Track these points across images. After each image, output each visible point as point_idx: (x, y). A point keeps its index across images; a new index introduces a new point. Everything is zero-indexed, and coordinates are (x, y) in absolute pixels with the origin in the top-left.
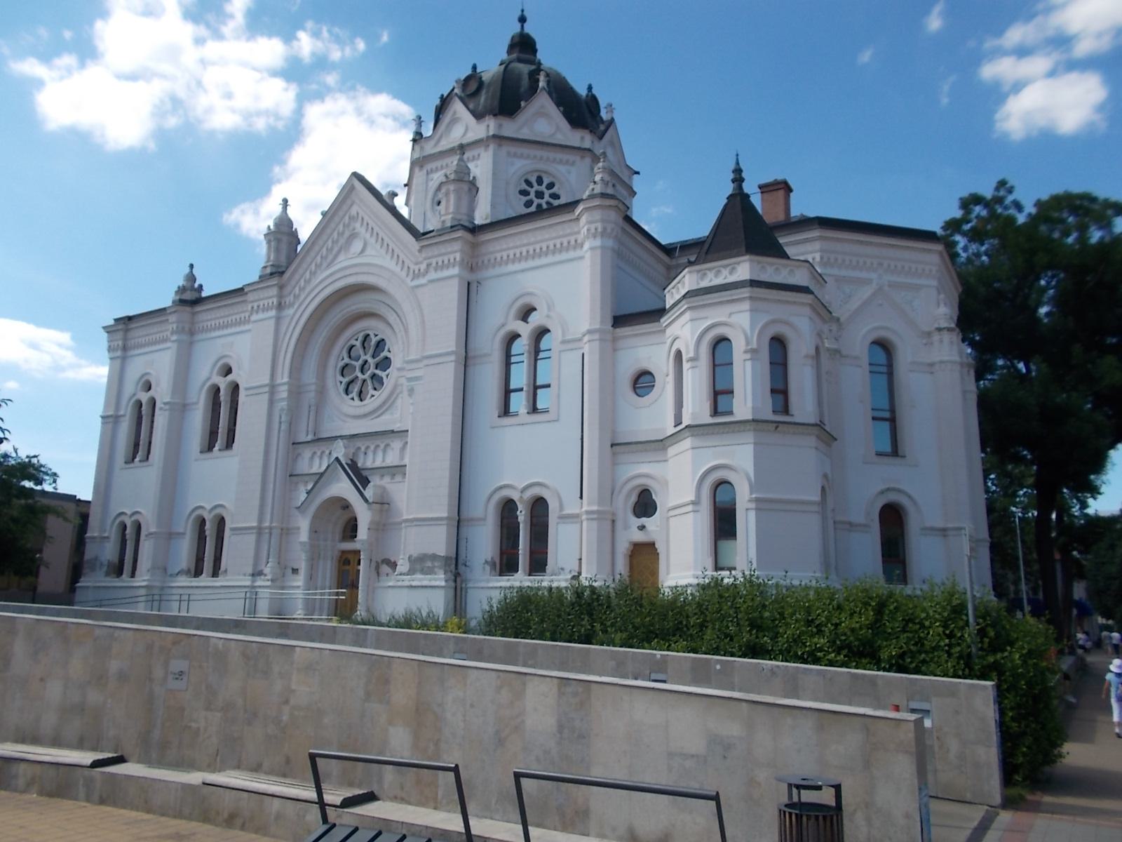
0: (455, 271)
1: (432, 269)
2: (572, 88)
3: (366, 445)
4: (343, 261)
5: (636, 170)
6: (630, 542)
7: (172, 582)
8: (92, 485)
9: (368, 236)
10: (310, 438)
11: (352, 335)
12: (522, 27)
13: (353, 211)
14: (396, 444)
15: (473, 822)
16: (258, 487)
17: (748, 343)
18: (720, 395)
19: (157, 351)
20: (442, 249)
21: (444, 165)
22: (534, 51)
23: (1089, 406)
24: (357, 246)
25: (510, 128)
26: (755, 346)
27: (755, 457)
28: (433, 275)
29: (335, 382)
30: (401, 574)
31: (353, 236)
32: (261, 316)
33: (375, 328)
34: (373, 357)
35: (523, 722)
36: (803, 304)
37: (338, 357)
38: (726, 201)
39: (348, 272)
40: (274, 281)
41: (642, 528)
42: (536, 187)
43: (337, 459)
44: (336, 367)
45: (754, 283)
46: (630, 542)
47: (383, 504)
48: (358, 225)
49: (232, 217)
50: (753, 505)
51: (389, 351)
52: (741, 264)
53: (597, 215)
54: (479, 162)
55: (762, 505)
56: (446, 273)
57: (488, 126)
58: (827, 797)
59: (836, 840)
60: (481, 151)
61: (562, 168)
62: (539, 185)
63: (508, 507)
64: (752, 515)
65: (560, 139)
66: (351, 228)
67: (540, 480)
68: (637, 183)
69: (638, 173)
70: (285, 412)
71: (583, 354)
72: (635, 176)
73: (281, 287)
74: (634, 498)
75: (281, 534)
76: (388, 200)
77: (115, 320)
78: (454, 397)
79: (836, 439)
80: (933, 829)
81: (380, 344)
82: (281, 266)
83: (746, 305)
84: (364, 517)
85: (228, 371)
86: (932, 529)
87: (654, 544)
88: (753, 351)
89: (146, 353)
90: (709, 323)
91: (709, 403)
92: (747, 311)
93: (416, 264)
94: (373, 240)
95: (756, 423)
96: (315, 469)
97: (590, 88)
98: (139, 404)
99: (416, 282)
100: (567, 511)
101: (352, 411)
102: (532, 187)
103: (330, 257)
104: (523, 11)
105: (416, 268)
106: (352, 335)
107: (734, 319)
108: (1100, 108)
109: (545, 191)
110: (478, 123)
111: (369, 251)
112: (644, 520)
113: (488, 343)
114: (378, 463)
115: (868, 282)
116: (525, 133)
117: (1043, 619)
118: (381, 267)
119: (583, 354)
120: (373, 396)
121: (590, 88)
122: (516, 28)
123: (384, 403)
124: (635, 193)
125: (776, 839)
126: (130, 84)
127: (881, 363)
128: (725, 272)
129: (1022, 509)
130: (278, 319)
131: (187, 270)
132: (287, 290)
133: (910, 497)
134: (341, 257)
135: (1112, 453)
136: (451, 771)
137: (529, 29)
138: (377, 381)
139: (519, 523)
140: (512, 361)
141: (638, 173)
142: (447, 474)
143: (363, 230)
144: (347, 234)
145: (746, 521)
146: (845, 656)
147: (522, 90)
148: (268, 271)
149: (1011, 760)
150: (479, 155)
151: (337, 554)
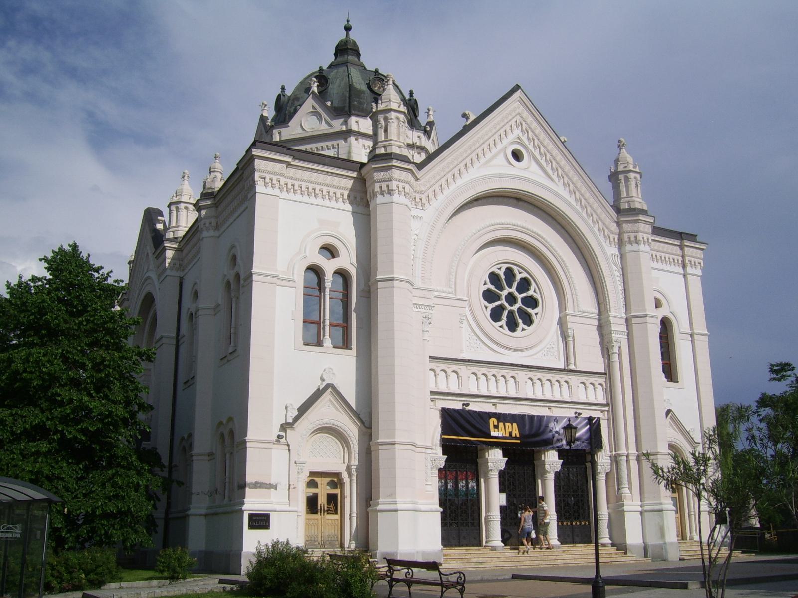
2: (307, 505)
7: (295, 146)
8: (661, 368)
12: (347, 35)
15: (408, 589)
16: (671, 246)
19: (443, 399)
21: (760, 442)
23: (43, 332)
34: (511, 313)
38: (462, 128)
42: (513, 290)
49: (758, 525)
51: (501, 327)
59: (720, 596)
62: (517, 289)
69: (259, 541)
78: (378, 478)
79: (696, 236)
80: (551, 541)
82: (122, 281)
89: (476, 401)
92: (698, 276)
97: (411, 93)
98: (315, 270)
102: (510, 286)
104: (348, 21)
108: (298, 548)
110: (338, 256)
117: (118, 314)
121: (411, 93)
122: (342, 35)
125: (592, 597)
126: (291, 451)
127: (339, 290)
129: (560, 524)
131: (279, 92)
135: (297, 413)
136: (346, 36)
137: (353, 35)
139: (507, 317)
140: (507, 424)
142: (380, 415)
146: (777, 455)
148: (246, 174)
149: (106, 282)
151: (566, 547)
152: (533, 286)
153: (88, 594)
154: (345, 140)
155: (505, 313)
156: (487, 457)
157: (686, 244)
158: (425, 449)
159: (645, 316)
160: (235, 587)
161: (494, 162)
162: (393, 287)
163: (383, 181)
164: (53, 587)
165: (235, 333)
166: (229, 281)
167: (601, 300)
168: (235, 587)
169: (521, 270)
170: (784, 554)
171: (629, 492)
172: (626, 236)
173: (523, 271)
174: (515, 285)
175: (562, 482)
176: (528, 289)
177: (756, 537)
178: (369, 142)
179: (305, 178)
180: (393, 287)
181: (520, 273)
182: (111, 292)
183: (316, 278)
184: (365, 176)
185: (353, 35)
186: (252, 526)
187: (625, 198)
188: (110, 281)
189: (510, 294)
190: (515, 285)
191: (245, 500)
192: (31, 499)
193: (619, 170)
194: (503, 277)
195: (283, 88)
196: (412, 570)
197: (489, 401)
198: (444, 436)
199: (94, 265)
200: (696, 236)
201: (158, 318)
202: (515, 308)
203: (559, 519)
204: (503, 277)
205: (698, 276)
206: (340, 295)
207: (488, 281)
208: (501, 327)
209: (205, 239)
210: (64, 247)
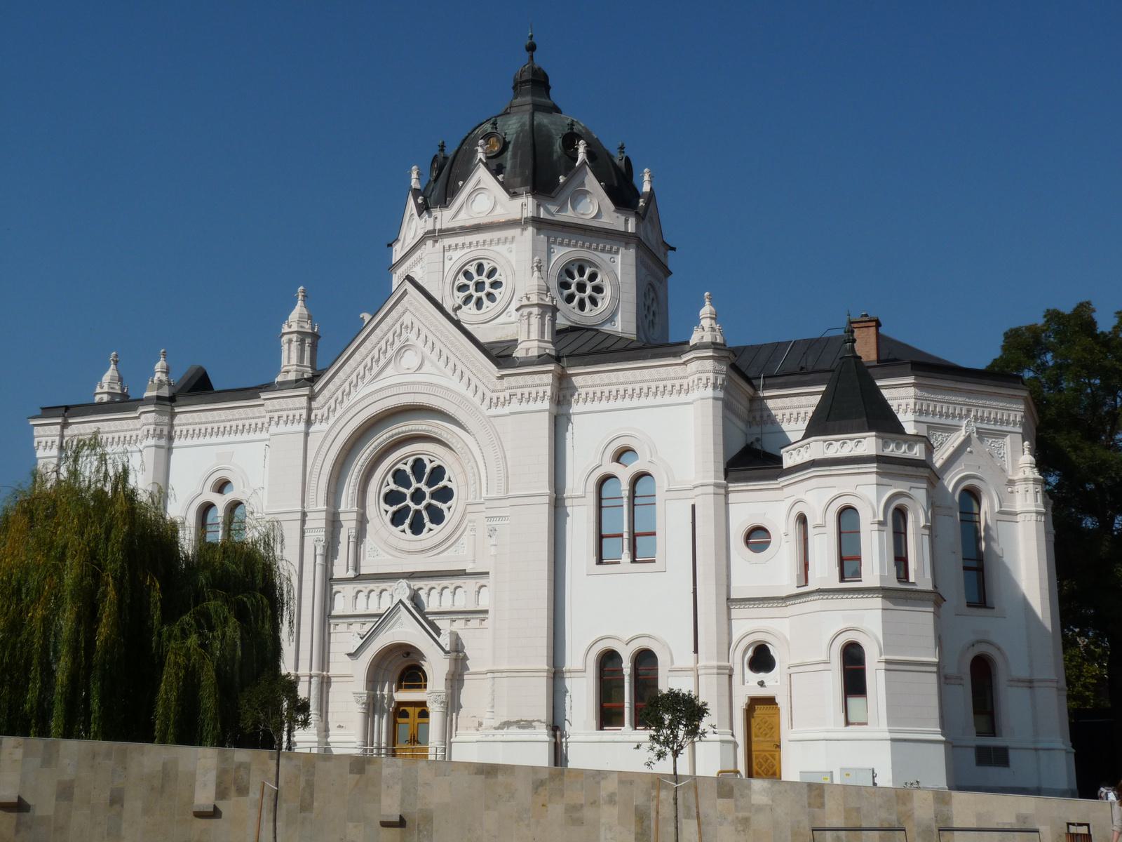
0: (546, 405)
1: (514, 400)
3: (429, 586)
4: (391, 376)
5: (672, 246)
6: (749, 697)
9: (427, 350)
10: (351, 574)
11: (402, 458)
13: (407, 319)
14: (470, 585)
17: (874, 516)
18: (848, 562)
20: (529, 379)
22: (548, 88)
24: (410, 359)
25: (550, 212)
26: (881, 519)
27: (883, 622)
28: (515, 406)
29: (378, 513)
30: (486, 729)
31: (405, 347)
32: (282, 428)
33: (432, 454)
34: (429, 484)
35: (913, 813)
36: (872, 436)
37: (381, 481)
39: (402, 389)
40: (306, 391)
41: (761, 684)
42: (577, 278)
43: (401, 601)
44: (379, 493)
45: (879, 459)
46: (749, 697)
47: (458, 657)
48: (413, 336)
50: (883, 666)
51: (450, 481)
52: (867, 439)
53: (709, 364)
54: (514, 246)
55: (892, 666)
56: (532, 406)
57: (524, 206)
58: (1083, 830)
60: (516, 232)
61: (501, 249)
63: (608, 660)
64: (881, 675)
65: (501, 214)
66: (402, 338)
67: (647, 632)
68: (672, 260)
69: (673, 249)
70: (322, 543)
71: (693, 507)
72: (670, 253)
73: (312, 398)
74: (750, 653)
75: (322, 683)
76: (452, 314)
77: (43, 409)
79: (945, 601)
81: (438, 473)
83: (873, 478)
84: (436, 667)
85: (222, 486)
86: (1019, 681)
87: (774, 699)
88: (880, 523)
90: (835, 492)
91: (838, 568)
92: (934, 672)
93: (493, 391)
94: (434, 356)
95: (885, 592)
96: (373, 609)
99: (493, 411)
100: (678, 664)
101: (406, 546)
103: (376, 369)
105: (495, 396)
106: (402, 458)
107: (861, 491)
109: (486, 280)
111: (424, 369)
112: (762, 676)
113: (579, 484)
114: (447, 606)
115: (955, 429)
116: (464, 219)
118: (448, 389)
119: (693, 507)
120: (431, 530)
123: (447, 539)
124: (670, 273)
128: (851, 444)
130: (307, 434)
132: (320, 400)
133: (999, 649)
134: (390, 370)
137: (541, 60)
138: (437, 517)
139: (624, 675)
141: (673, 249)
143: (420, 343)
144: (397, 345)
145: (875, 676)
147: (555, 157)
150: (513, 238)
152: (385, 490)
153: (346, 478)
154: (295, 744)
155: (434, 502)
156: (1115, 792)
157: (176, 411)
158: (531, 327)
159: (893, 740)
160: (160, 654)
161: (384, 375)
162: (883, 609)
163: (925, 400)
164: (497, 165)
165: (447, 716)
166: (419, 216)
167: (439, 574)
168: (160, 654)
169: (385, 483)
170: (618, 363)
171: (619, 318)
172: (177, 429)
173: (386, 481)
174: (412, 479)
175: (120, 449)
176: (392, 491)
177: (421, 682)
178: (877, 572)
179: (370, 347)
180: (883, 609)
181: (388, 485)
182: (901, 795)
183: (461, 702)
184: (574, 414)
185: (534, 40)
186: (857, 574)
187: (286, 366)
188: (1043, 510)
189: (418, 490)
190: (412, 479)
191: (330, 733)
192: (393, 291)
193: (929, 587)
194: (408, 521)
195: (442, 147)
196: (553, 303)
197: (477, 616)
198: (847, 667)
199: (294, 736)
200: (945, 601)
201: (430, 163)
202: (408, 502)
203: (623, 706)
204: (408, 521)
205: (934, 672)
206: (209, 528)
207: (425, 530)
208: (450, 481)
209: (984, 354)
210: (132, 481)
